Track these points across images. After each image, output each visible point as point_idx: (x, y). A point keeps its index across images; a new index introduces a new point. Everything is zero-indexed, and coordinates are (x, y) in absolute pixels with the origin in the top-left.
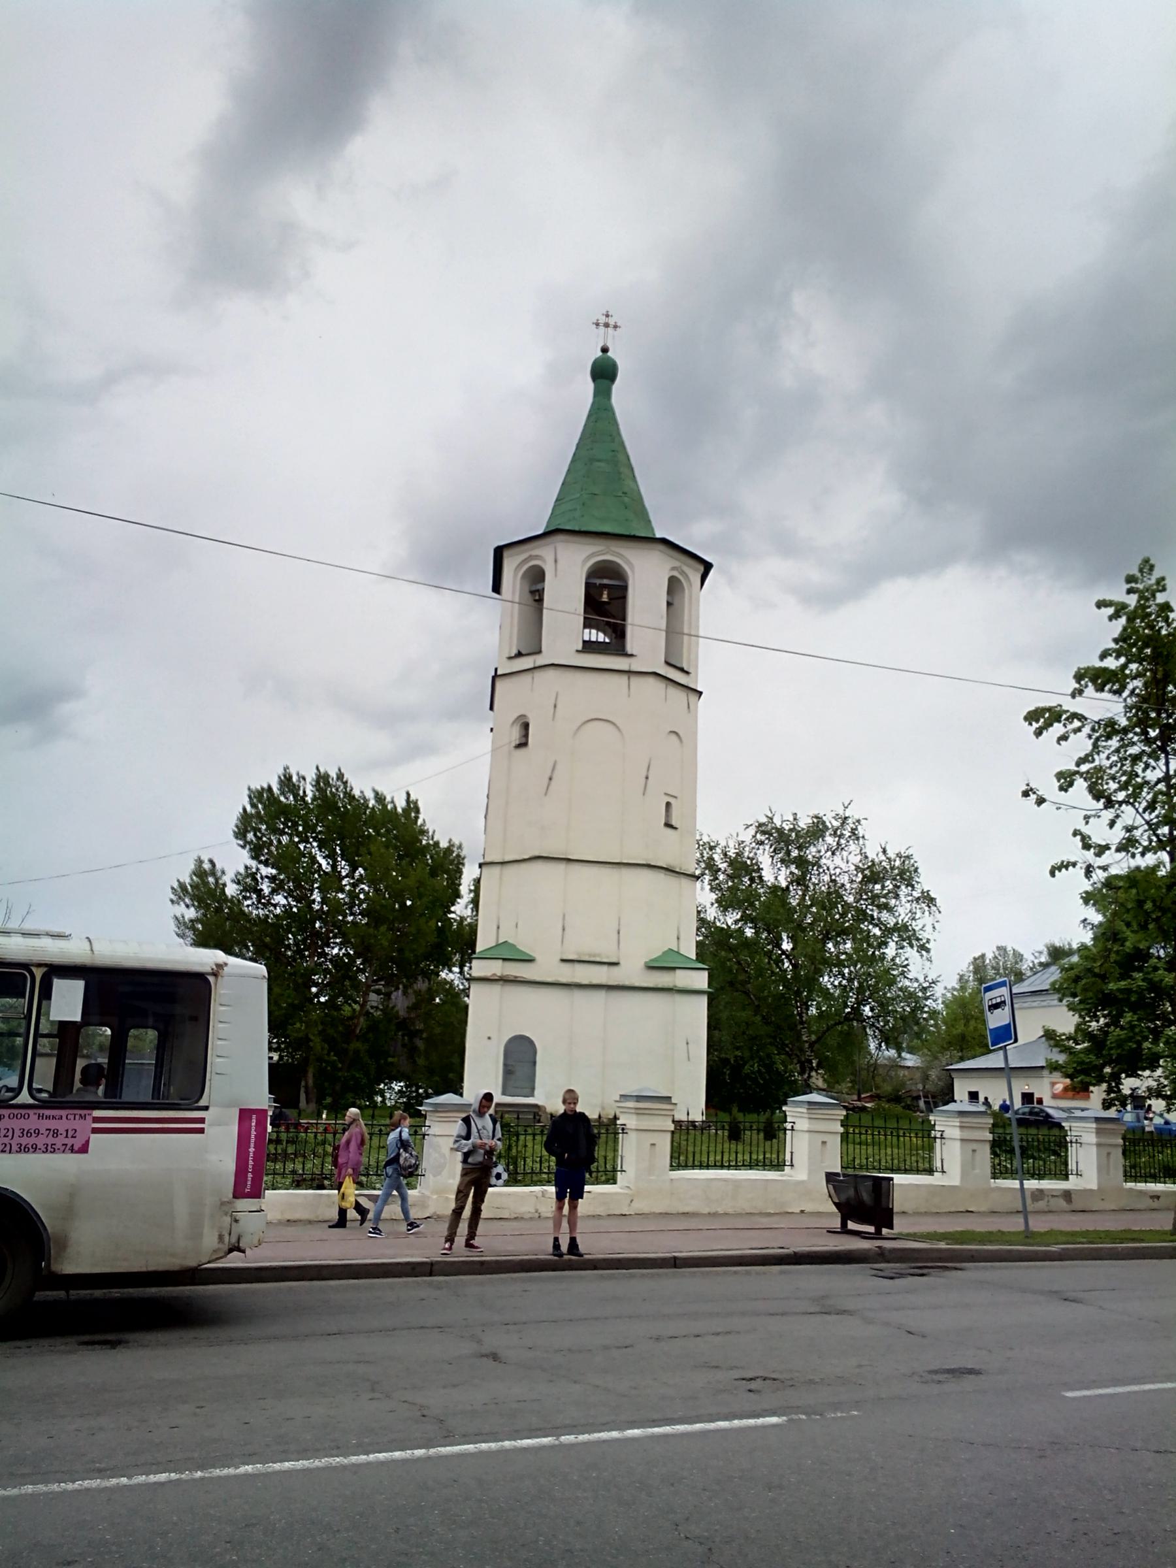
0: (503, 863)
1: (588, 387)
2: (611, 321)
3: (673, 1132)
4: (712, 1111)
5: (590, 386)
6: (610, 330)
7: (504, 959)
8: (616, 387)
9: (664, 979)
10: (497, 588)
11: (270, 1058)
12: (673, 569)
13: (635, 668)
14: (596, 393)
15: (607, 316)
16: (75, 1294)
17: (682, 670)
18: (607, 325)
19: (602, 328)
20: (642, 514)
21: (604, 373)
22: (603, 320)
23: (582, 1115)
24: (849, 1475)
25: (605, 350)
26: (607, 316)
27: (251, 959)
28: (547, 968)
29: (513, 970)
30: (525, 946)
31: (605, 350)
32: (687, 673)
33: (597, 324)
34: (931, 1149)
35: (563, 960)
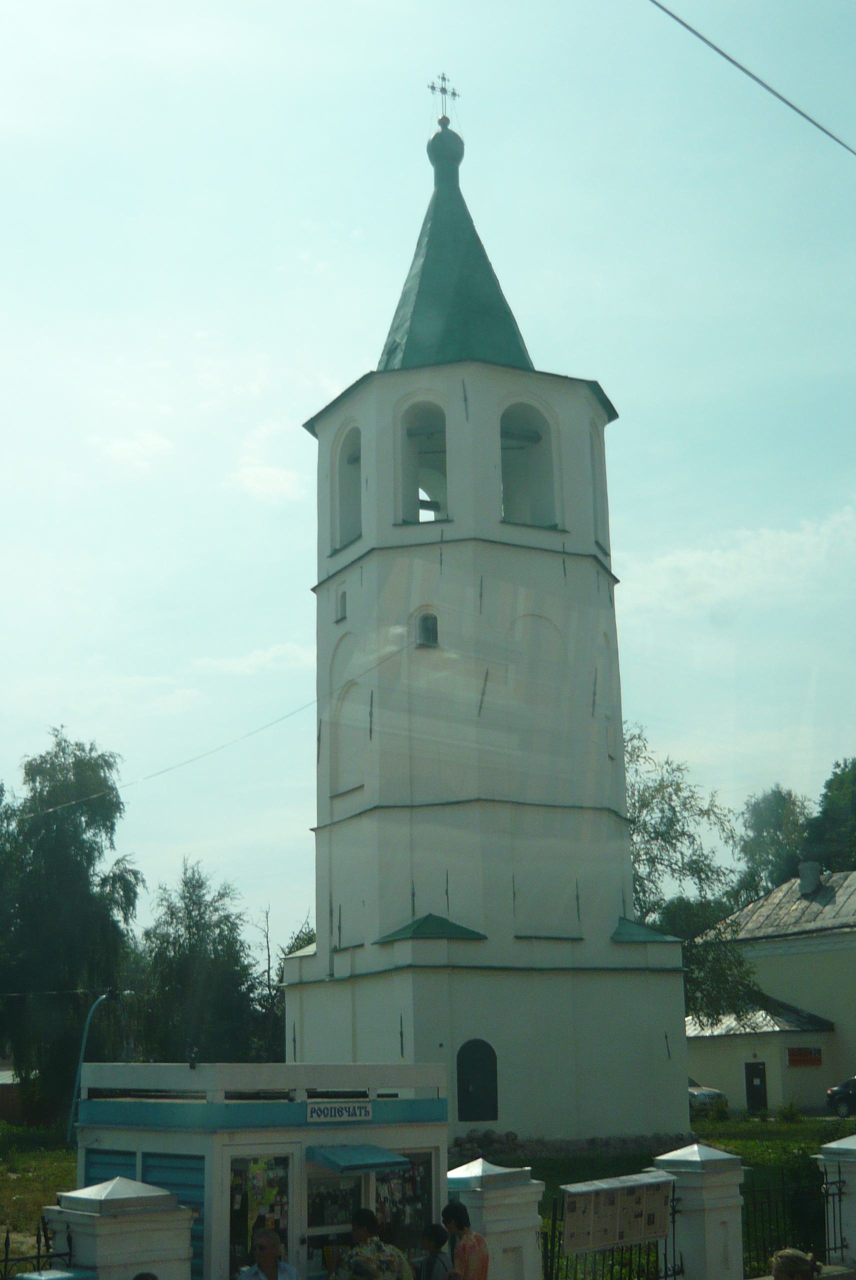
2: (449, 87)
6: (448, 97)
10: (681, 1253)
11: (256, 1161)
15: (444, 79)
16: (674, 1170)
17: (554, 528)
18: (444, 91)
19: (438, 93)
21: (446, 151)
22: (439, 84)
23: (430, 917)
24: (584, 1212)
25: (444, 122)
26: (444, 79)
27: (144, 1062)
28: (500, 949)
29: (465, 953)
31: (444, 122)
32: (564, 531)
33: (433, 88)
35: (518, 938)
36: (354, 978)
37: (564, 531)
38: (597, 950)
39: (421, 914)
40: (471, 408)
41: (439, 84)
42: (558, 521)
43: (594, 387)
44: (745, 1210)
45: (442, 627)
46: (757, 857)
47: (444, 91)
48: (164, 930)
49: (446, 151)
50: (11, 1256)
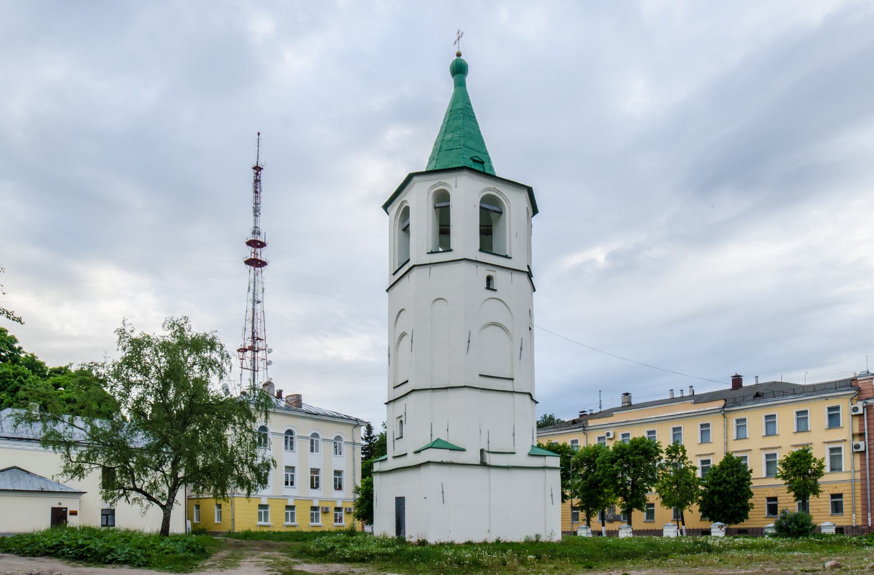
8: (469, 80)
17: (506, 257)
25: (459, 55)
42: (508, 253)
43: (530, 191)
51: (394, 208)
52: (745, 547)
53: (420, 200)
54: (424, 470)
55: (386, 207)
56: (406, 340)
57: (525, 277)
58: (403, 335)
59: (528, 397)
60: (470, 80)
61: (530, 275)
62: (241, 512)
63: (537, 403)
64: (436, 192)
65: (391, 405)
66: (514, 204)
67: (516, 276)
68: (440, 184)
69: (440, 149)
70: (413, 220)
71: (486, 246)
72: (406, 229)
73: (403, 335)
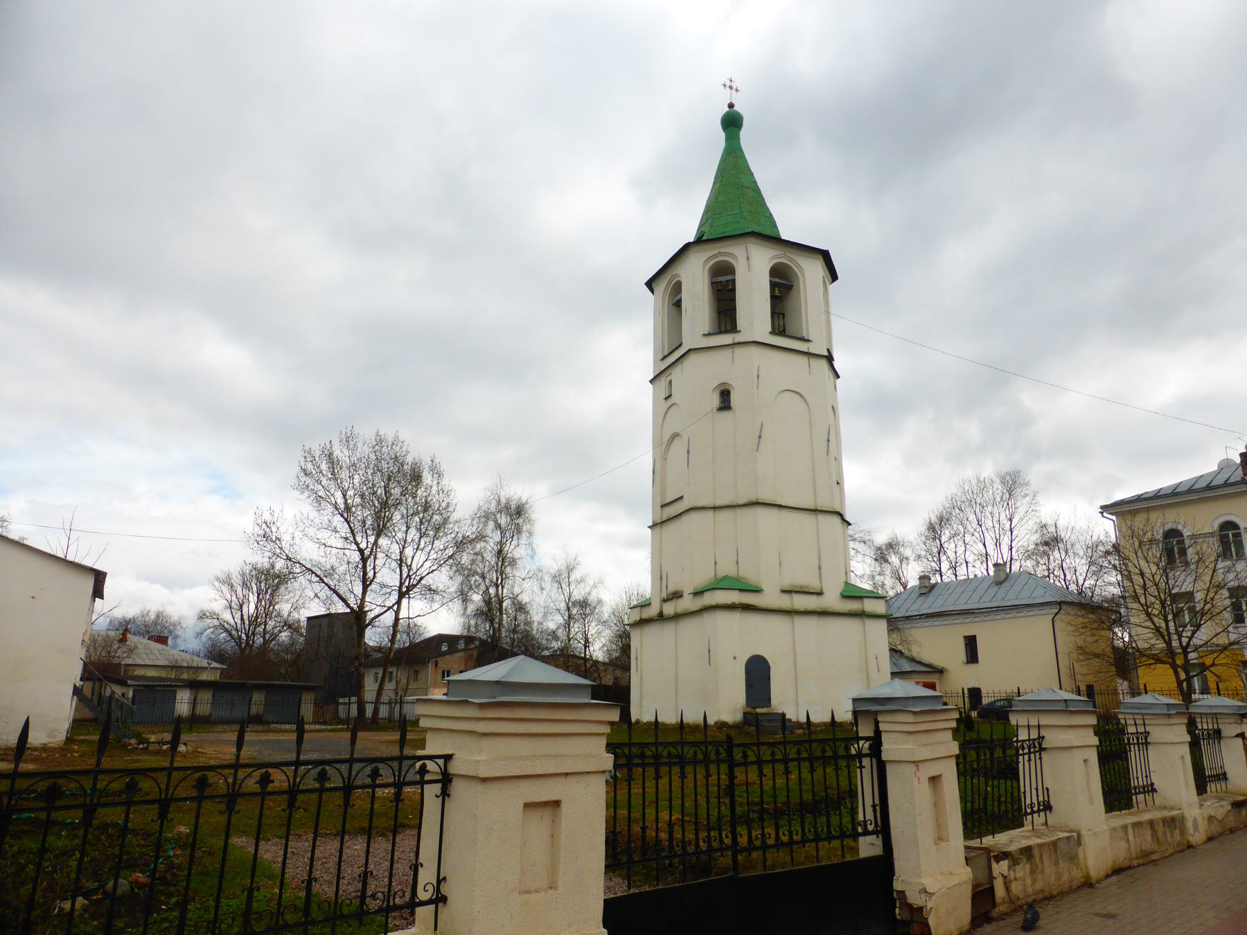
0: (715, 508)
1: (721, 135)
3: (957, 757)
4: (624, 683)
5: (722, 135)
7: (741, 590)
8: (743, 133)
9: (854, 606)
12: (774, 257)
13: (812, 351)
14: (727, 139)
17: (803, 339)
18: (731, 87)
20: (774, 224)
22: (728, 83)
25: (731, 106)
28: (771, 598)
30: (749, 573)
31: (731, 106)
32: (808, 341)
34: (1011, 772)
35: (783, 591)
36: (677, 617)
37: (808, 341)
38: (831, 600)
39: (721, 574)
40: (753, 270)
41: (728, 83)
42: (805, 335)
43: (825, 256)
44: (961, 760)
45: (735, 399)
46: (283, 670)
47: (731, 87)
48: (471, 608)
49: (732, 122)
50: (195, 805)
51: (661, 287)
52: (318, 731)
53: (696, 281)
54: (685, 518)
55: (650, 284)
56: (679, 447)
57: (824, 363)
58: (675, 436)
59: (837, 520)
60: (746, 136)
61: (830, 359)
62: (327, 785)
63: (849, 524)
64: (711, 268)
65: (658, 529)
66: (810, 273)
67: (814, 361)
68: (720, 254)
69: (713, 210)
70: (685, 295)
71: (779, 329)
72: (678, 304)
73: (675, 436)
